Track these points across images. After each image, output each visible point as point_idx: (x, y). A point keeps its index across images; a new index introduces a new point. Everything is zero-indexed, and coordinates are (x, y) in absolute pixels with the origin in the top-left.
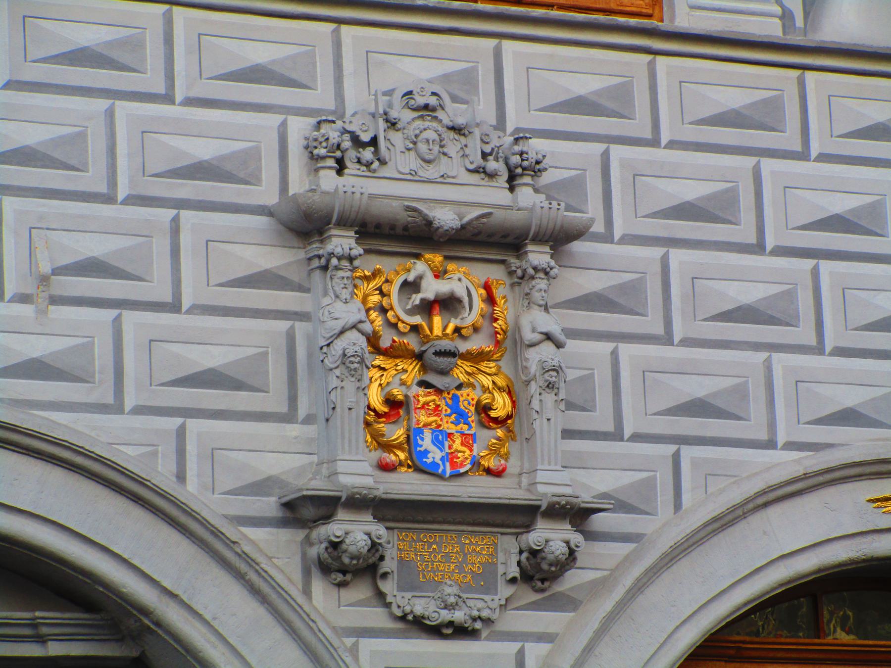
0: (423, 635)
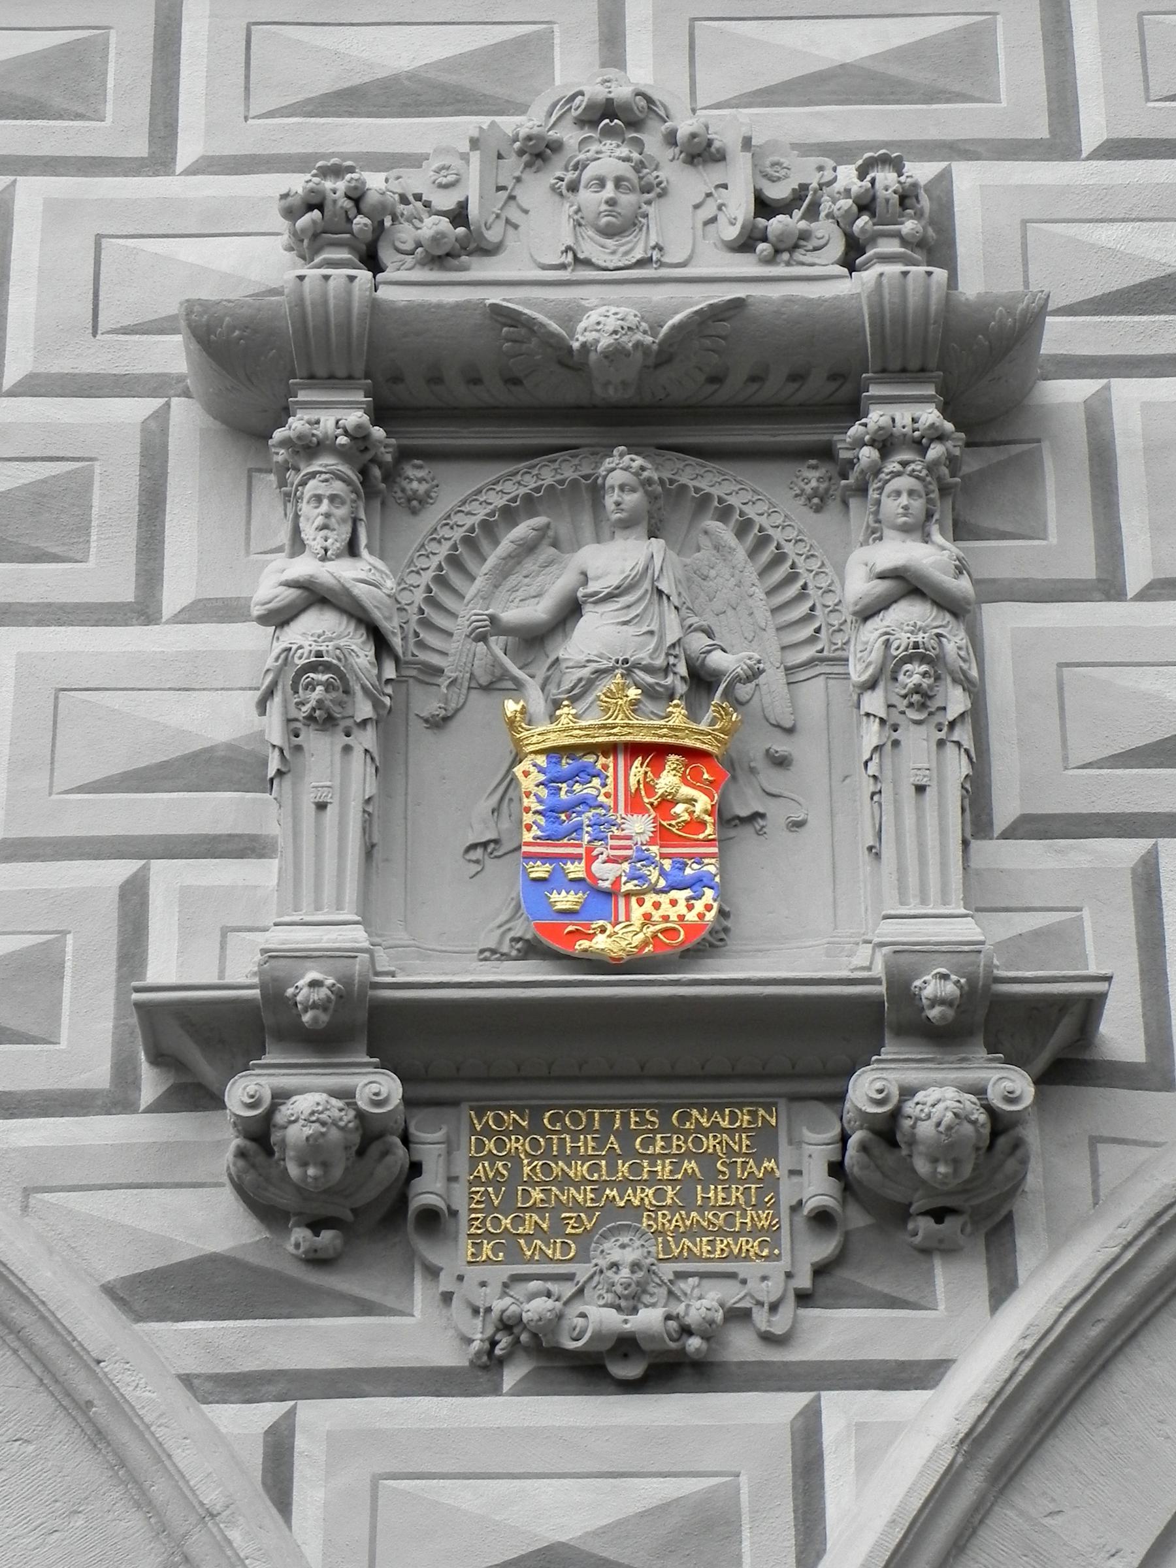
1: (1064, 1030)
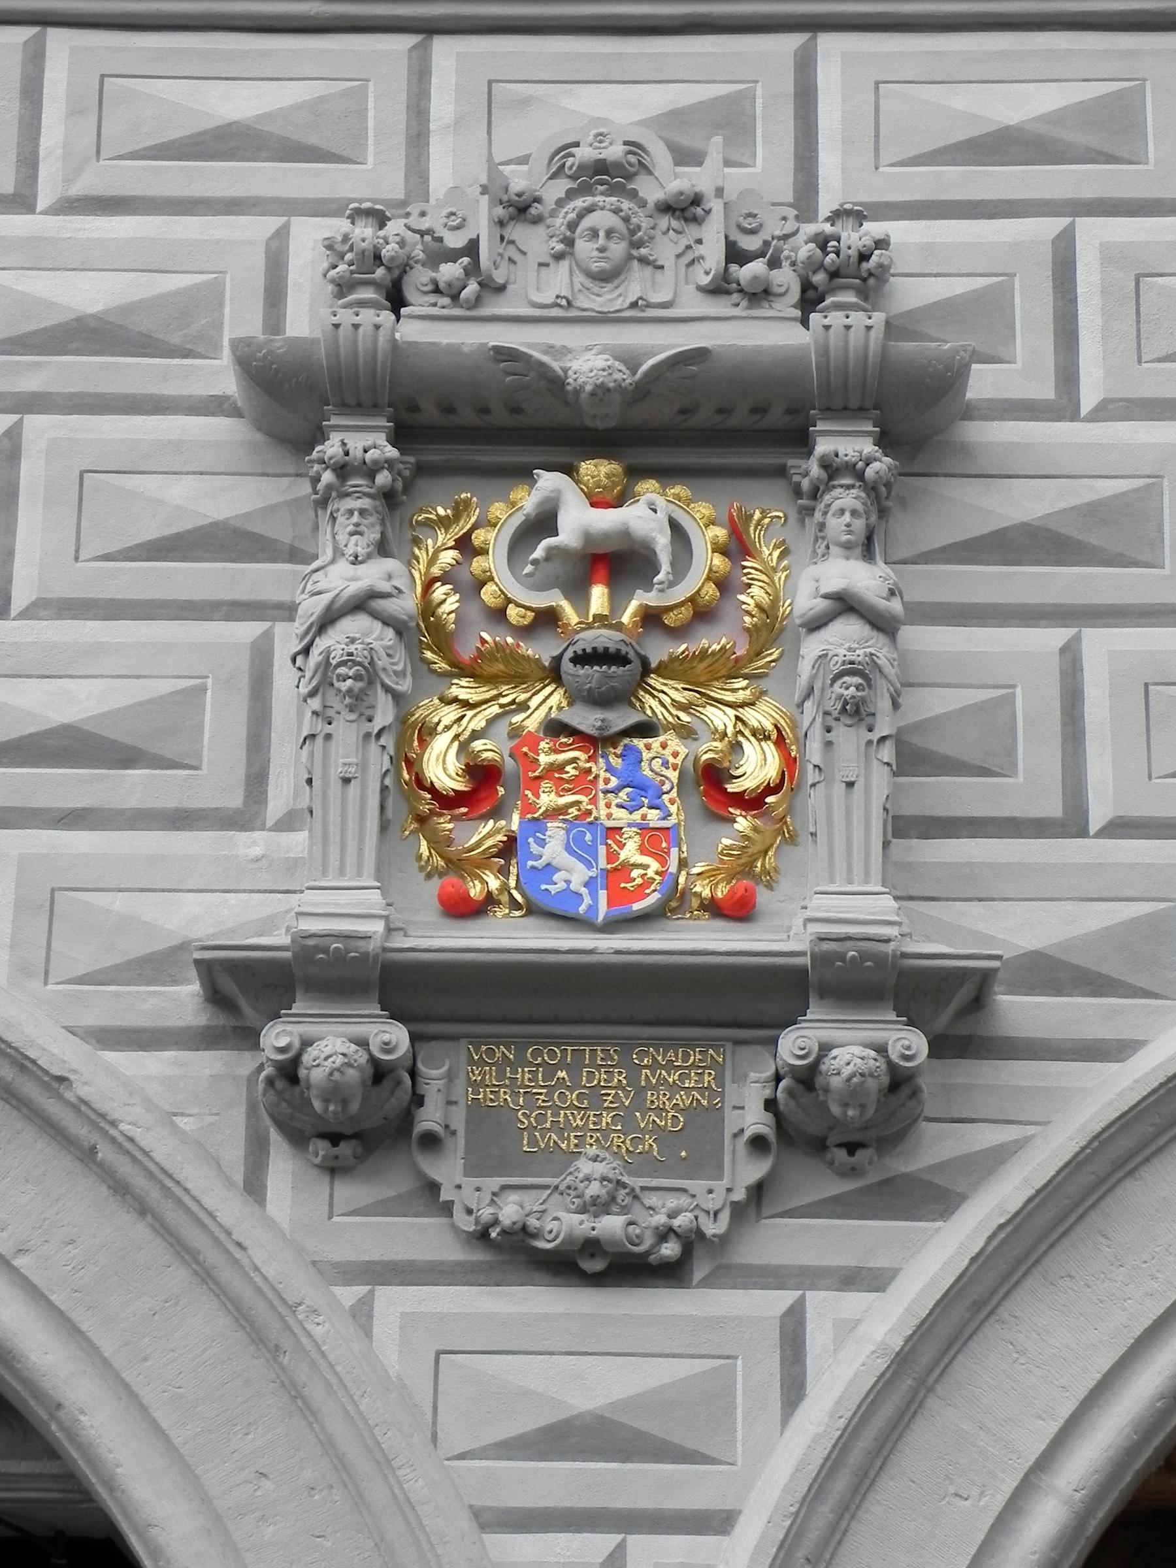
0: (539, 1276)
1: (963, 996)
